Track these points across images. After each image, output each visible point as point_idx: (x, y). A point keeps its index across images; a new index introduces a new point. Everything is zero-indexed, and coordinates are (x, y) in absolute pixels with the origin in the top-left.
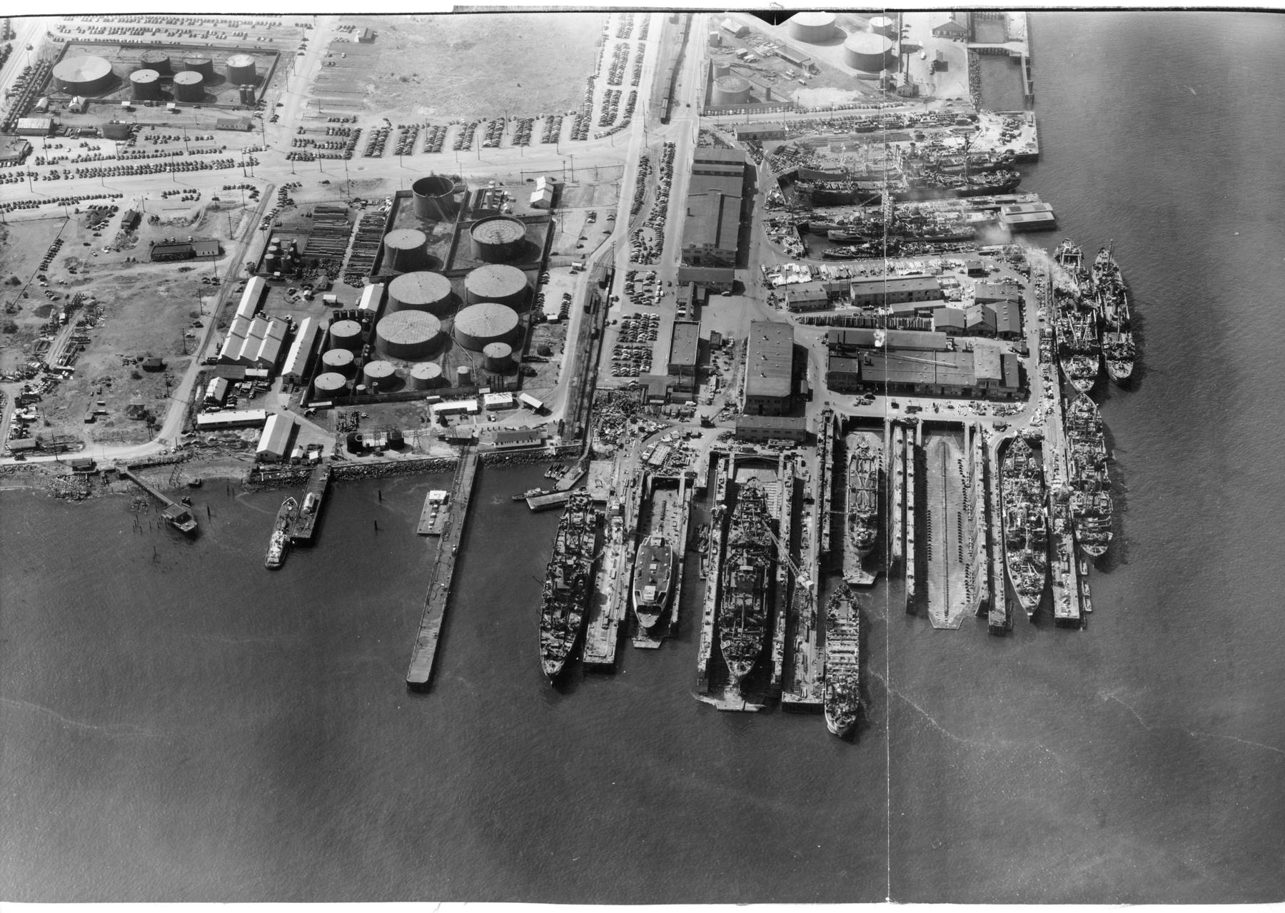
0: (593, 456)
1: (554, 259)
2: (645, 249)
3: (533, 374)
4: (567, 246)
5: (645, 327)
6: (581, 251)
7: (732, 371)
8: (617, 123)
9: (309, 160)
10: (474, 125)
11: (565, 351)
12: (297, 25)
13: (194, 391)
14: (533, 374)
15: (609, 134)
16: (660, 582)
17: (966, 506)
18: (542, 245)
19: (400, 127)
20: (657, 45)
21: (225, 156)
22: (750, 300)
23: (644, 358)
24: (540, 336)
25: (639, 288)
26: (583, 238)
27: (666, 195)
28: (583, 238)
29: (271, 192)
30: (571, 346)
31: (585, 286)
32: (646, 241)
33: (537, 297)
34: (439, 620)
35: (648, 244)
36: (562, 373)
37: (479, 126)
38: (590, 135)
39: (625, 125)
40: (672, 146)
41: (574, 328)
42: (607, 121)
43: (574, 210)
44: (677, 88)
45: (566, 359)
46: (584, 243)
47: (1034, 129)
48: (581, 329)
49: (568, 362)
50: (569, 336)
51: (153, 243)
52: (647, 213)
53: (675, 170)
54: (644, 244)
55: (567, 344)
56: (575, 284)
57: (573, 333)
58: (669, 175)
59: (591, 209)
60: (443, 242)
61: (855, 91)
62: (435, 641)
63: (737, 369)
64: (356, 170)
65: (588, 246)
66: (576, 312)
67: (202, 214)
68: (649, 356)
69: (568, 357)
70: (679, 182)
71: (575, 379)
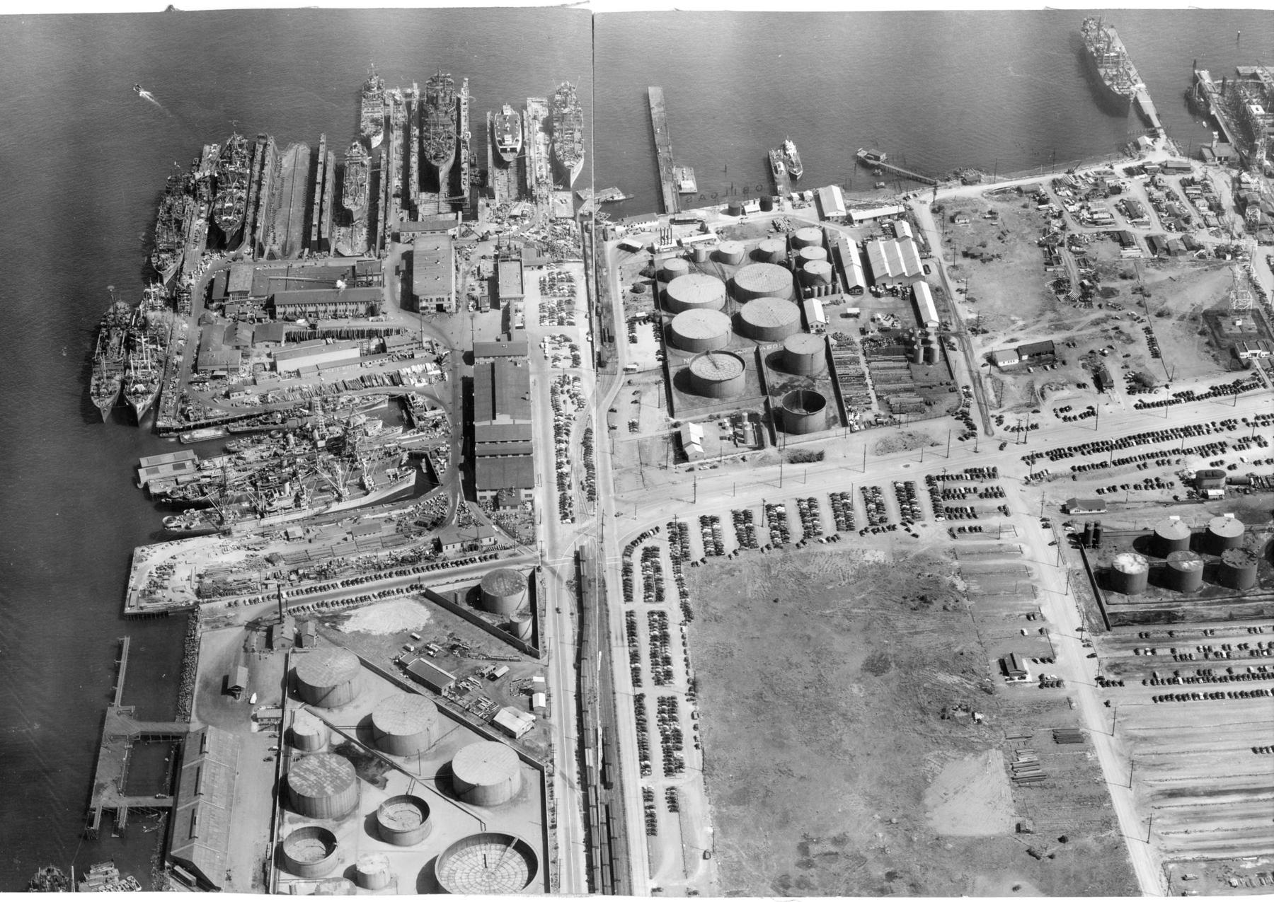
0: (573, 219)
1: (659, 378)
2: (568, 391)
3: (642, 274)
4: (649, 393)
5: (552, 312)
6: (632, 389)
7: (467, 285)
8: (638, 553)
9: (991, 496)
10: (807, 535)
11: (620, 295)
12: (1121, 684)
13: (925, 239)
14: (642, 274)
15: (644, 536)
16: (502, 119)
17: (272, 212)
18: (674, 391)
19: (894, 528)
20: (617, 689)
21: (1064, 465)
22: (457, 347)
23: (547, 287)
24: (646, 306)
25: (565, 351)
26: (635, 402)
27: (559, 452)
28: (635, 402)
29: (986, 428)
30: (617, 299)
31: (620, 354)
32: (569, 401)
33: (662, 338)
34: (653, 116)
35: (566, 396)
36: (619, 278)
37: (801, 537)
38: (665, 534)
39: (628, 552)
40: (565, 516)
41: (619, 315)
42: (650, 553)
43: (655, 434)
44: (575, 610)
45: (619, 290)
46: (634, 398)
47: (132, 583)
48: (612, 315)
49: (615, 285)
50: (622, 308)
51: (1064, 363)
52: (575, 438)
53: (555, 487)
54: (570, 397)
55: (621, 301)
56: (630, 355)
57: (618, 310)
58: (561, 476)
59: (636, 436)
60: (777, 386)
61: (347, 631)
62: (652, 106)
63: (463, 285)
64: (911, 464)
65: (628, 392)
66: (621, 331)
67: (1040, 399)
68: (543, 289)
69: (616, 290)
70: (547, 461)
71: (605, 274)
